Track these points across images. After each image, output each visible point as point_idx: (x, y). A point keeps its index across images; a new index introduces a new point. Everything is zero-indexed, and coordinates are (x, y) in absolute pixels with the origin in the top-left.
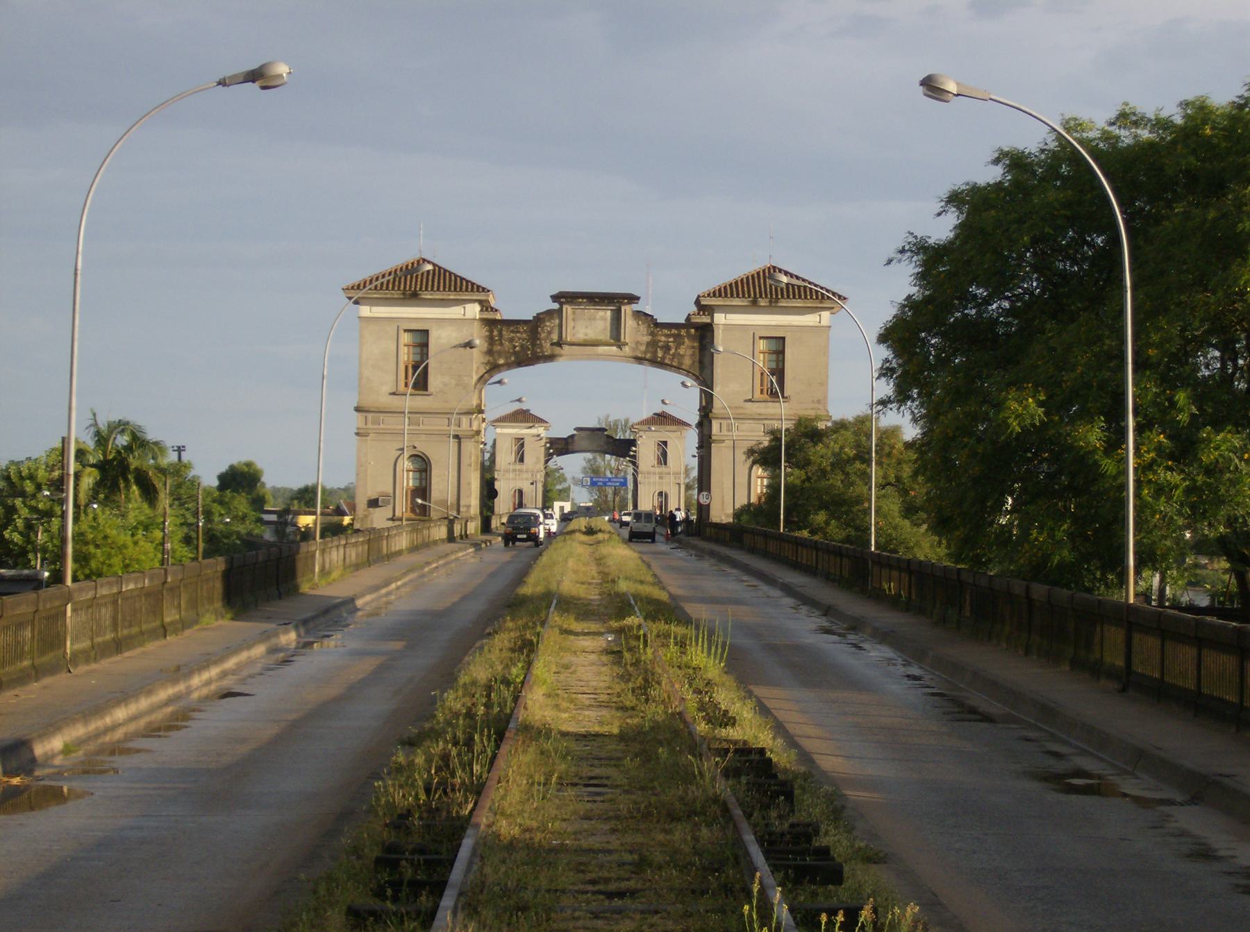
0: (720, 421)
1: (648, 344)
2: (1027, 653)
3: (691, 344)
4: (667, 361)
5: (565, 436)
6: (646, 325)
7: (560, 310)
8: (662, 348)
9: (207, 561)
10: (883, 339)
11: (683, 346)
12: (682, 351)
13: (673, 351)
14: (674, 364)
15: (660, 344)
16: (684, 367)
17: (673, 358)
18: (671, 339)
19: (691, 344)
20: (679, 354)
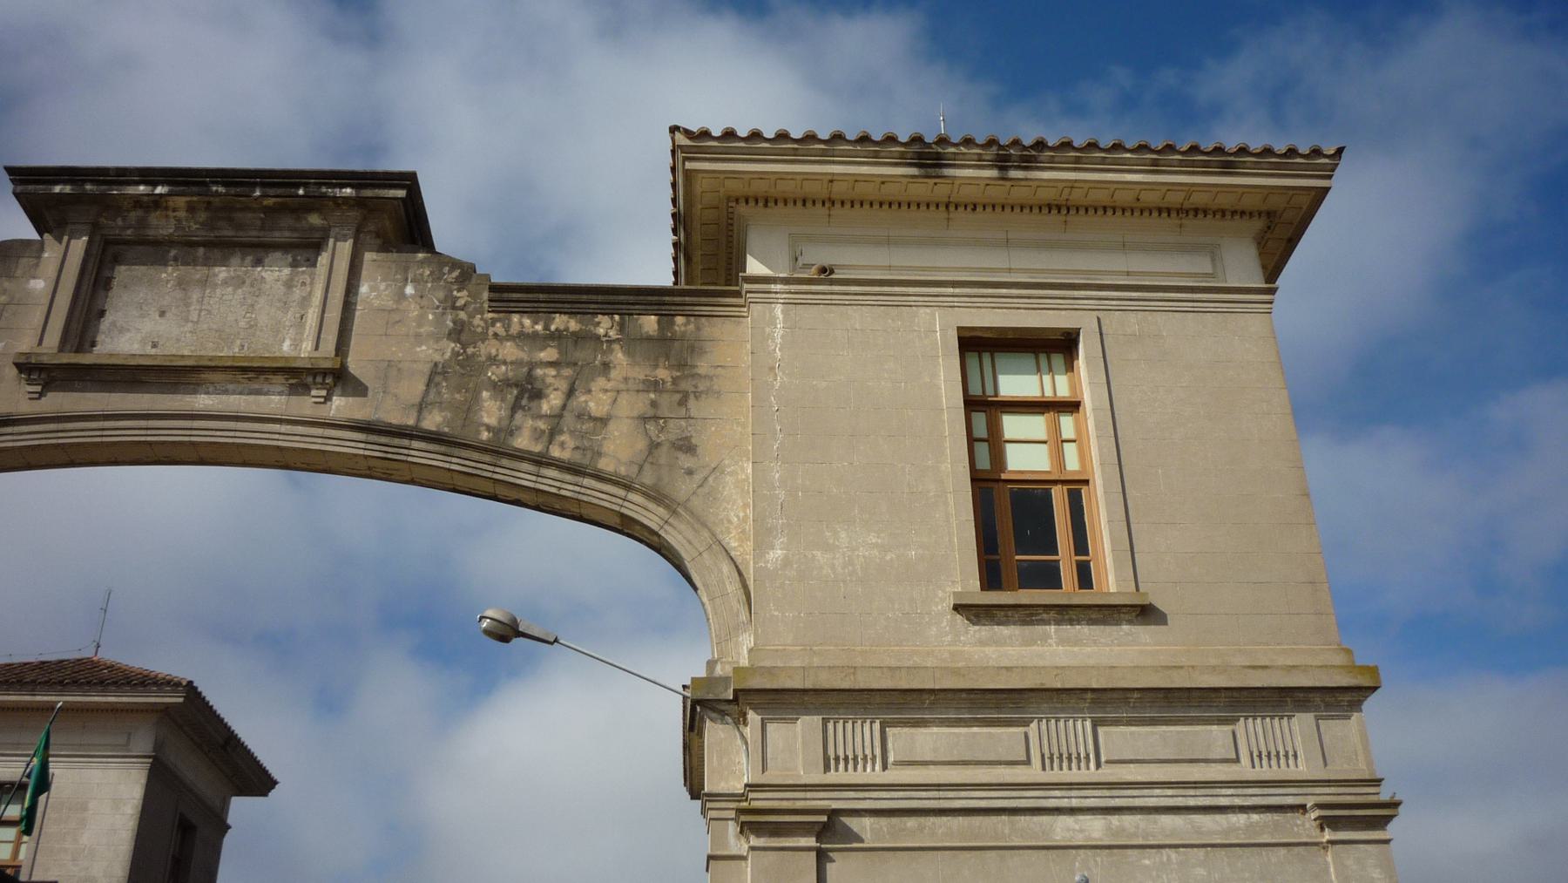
0: (1084, 598)
1: (436, 374)
2: (686, 446)
3: (640, 373)
4: (522, 442)
5: (521, 638)
6: (437, 297)
7: (41, 247)
8: (499, 387)
9: (1094, 587)
10: (692, 679)
11: (601, 382)
12: (596, 401)
13: (552, 402)
14: (556, 452)
15: (494, 373)
16: (606, 465)
17: (553, 433)
18: (550, 354)
19: (640, 373)
20: (582, 415)
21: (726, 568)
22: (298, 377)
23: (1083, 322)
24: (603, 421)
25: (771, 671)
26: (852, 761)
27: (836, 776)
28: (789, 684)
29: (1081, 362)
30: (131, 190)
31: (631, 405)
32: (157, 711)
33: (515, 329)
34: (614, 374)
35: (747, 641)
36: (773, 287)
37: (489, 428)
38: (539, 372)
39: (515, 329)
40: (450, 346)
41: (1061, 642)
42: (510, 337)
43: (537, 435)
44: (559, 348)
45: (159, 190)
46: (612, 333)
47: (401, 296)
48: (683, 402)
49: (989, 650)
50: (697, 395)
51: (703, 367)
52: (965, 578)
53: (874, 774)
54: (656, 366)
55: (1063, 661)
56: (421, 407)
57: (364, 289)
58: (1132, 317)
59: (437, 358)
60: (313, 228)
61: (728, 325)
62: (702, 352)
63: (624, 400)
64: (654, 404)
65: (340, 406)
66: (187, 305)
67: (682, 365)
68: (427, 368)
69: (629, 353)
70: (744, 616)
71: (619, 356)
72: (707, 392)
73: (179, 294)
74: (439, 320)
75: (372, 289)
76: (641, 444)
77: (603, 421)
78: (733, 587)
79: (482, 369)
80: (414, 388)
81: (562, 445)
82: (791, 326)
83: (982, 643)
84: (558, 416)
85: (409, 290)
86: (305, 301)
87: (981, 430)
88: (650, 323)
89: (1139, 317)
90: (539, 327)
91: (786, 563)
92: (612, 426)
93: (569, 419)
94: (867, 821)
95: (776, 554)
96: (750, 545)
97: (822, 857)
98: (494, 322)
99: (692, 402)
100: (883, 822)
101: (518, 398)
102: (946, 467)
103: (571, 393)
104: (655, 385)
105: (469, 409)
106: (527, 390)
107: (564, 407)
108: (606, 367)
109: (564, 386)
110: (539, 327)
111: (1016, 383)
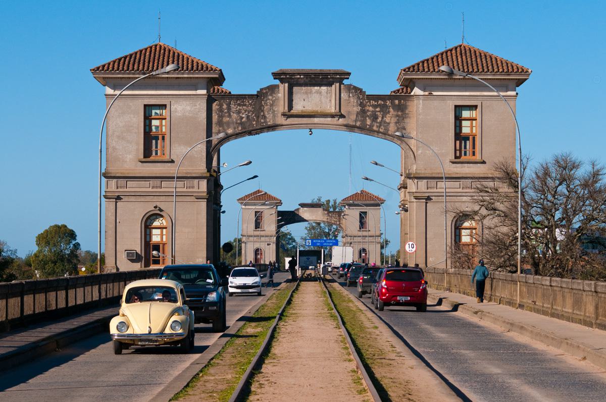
12: (387, 119)
13: (379, 119)
21: (411, 153)
22: (333, 116)
23: (478, 103)
24: (389, 123)
25: (419, 174)
26: (432, 188)
27: (429, 190)
28: (421, 176)
29: (477, 110)
30: (296, 77)
31: (394, 120)
32: (508, 323)
33: (372, 104)
34: (390, 113)
35: (415, 167)
36: (420, 97)
37: (368, 125)
38: (377, 113)
39: (372, 104)
40: (360, 108)
41: (468, 167)
42: (370, 106)
43: (377, 126)
44: (380, 108)
45: (302, 77)
46: (390, 104)
47: (349, 97)
48: (403, 119)
49: (455, 169)
50: (406, 118)
51: (407, 112)
52: (452, 157)
53: (435, 190)
54: (398, 112)
55: (467, 172)
56: (356, 121)
57: (342, 95)
58: (488, 102)
59: (358, 110)
60: (331, 81)
61: (412, 102)
62: (407, 109)
63: (393, 119)
64: (398, 120)
65: (341, 121)
66: (309, 98)
67: (402, 111)
68: (356, 113)
69: (393, 109)
70: (414, 162)
71: (391, 110)
72: (408, 117)
73: (306, 95)
74: (357, 101)
75: (344, 95)
76: (396, 128)
77: (389, 123)
78: (412, 156)
79: (366, 113)
80: (354, 117)
81: (382, 129)
82: (423, 105)
83: (454, 168)
84: (380, 123)
85: (351, 95)
86: (331, 96)
87: (458, 124)
88: (397, 102)
89: (337, 302)
90: (376, 103)
91: (422, 153)
92: (391, 124)
93: (383, 123)
94: (434, 197)
95: (420, 152)
96: (415, 148)
97: (426, 203)
98: (367, 102)
99: (405, 119)
100: (436, 197)
101: (373, 119)
102: (450, 134)
103: (382, 118)
104: (397, 116)
105: (364, 121)
106: (375, 118)
107: (382, 121)
108: (389, 112)
109: (381, 116)
110: (376, 103)
111: (466, 114)
